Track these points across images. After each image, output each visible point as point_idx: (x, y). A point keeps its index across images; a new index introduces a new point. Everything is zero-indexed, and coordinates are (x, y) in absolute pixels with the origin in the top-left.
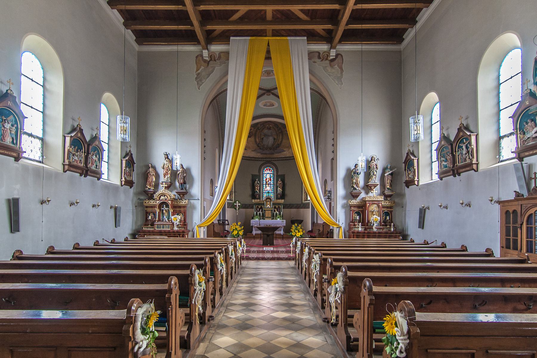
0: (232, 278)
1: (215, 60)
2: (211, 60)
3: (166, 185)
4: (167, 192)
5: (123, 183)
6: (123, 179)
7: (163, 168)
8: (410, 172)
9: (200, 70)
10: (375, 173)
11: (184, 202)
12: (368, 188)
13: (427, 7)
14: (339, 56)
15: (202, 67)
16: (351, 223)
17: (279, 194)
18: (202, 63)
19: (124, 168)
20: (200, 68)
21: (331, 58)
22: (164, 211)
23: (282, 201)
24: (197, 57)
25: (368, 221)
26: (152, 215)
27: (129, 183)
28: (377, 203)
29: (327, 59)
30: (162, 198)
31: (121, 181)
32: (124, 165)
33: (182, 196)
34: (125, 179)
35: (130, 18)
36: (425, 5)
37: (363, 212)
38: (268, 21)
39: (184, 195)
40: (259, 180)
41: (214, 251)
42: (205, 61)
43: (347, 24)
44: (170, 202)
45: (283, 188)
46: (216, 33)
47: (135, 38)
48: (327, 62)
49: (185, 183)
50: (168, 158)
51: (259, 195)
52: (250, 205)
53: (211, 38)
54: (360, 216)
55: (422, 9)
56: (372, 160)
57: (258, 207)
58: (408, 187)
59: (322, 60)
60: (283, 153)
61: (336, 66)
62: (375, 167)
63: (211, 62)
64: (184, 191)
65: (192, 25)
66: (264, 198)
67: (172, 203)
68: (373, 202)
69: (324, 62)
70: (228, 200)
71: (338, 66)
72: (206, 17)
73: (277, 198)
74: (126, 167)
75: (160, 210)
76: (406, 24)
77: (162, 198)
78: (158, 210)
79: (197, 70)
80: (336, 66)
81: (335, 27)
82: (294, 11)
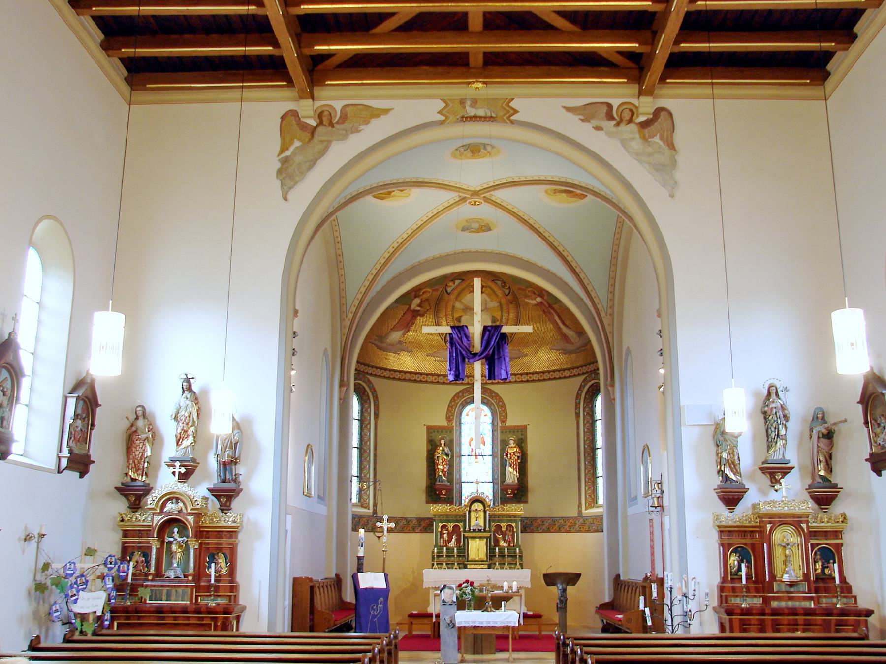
0: (568, 109)
1: (331, 125)
2: (321, 123)
3: (183, 470)
4: (183, 488)
5: (64, 463)
6: (66, 452)
7: (176, 418)
8: (878, 430)
9: (292, 149)
10: (782, 432)
11: (227, 520)
12: (775, 472)
13: (846, 49)
14: (663, 114)
15: (297, 143)
16: (728, 584)
17: (509, 486)
18: (299, 132)
19: (69, 421)
20: (291, 143)
21: (642, 119)
22: (174, 548)
23: (516, 509)
24: (283, 118)
25: (773, 577)
26: (138, 556)
27: (80, 463)
28: (795, 521)
29: (630, 121)
30: (170, 506)
31: (59, 458)
32: (70, 412)
33: (223, 500)
34: (71, 452)
35: (115, 32)
36: (840, 46)
37: (757, 550)
38: (472, 33)
39: (230, 498)
40: (450, 444)
41: (371, 647)
42: (304, 127)
43: (677, 42)
44: (191, 519)
45: (522, 468)
46: (335, 61)
47: (102, 37)
48: (633, 127)
49: (234, 461)
50: (190, 389)
51: (450, 490)
52: (420, 520)
53: (318, 69)
54: (749, 562)
55: (835, 53)
56: (769, 394)
57: (443, 527)
58: (879, 474)
59: (618, 124)
60: (519, 361)
61: (657, 139)
62: (780, 413)
63: (321, 129)
64: (231, 486)
65: (276, 44)
66: (465, 500)
67: (196, 522)
68: (781, 520)
69: (623, 127)
70: (355, 505)
71: (661, 138)
72: (312, 27)
73: (505, 501)
74: (76, 416)
75: (163, 542)
76: (831, 42)
77: (170, 506)
78: (155, 544)
79: (282, 151)
80: (657, 139)
81: (665, 5)
82: (538, 14)
